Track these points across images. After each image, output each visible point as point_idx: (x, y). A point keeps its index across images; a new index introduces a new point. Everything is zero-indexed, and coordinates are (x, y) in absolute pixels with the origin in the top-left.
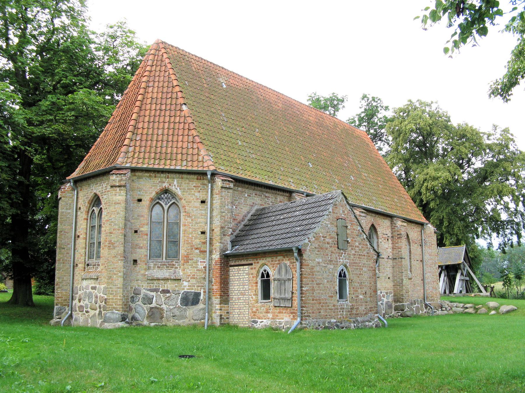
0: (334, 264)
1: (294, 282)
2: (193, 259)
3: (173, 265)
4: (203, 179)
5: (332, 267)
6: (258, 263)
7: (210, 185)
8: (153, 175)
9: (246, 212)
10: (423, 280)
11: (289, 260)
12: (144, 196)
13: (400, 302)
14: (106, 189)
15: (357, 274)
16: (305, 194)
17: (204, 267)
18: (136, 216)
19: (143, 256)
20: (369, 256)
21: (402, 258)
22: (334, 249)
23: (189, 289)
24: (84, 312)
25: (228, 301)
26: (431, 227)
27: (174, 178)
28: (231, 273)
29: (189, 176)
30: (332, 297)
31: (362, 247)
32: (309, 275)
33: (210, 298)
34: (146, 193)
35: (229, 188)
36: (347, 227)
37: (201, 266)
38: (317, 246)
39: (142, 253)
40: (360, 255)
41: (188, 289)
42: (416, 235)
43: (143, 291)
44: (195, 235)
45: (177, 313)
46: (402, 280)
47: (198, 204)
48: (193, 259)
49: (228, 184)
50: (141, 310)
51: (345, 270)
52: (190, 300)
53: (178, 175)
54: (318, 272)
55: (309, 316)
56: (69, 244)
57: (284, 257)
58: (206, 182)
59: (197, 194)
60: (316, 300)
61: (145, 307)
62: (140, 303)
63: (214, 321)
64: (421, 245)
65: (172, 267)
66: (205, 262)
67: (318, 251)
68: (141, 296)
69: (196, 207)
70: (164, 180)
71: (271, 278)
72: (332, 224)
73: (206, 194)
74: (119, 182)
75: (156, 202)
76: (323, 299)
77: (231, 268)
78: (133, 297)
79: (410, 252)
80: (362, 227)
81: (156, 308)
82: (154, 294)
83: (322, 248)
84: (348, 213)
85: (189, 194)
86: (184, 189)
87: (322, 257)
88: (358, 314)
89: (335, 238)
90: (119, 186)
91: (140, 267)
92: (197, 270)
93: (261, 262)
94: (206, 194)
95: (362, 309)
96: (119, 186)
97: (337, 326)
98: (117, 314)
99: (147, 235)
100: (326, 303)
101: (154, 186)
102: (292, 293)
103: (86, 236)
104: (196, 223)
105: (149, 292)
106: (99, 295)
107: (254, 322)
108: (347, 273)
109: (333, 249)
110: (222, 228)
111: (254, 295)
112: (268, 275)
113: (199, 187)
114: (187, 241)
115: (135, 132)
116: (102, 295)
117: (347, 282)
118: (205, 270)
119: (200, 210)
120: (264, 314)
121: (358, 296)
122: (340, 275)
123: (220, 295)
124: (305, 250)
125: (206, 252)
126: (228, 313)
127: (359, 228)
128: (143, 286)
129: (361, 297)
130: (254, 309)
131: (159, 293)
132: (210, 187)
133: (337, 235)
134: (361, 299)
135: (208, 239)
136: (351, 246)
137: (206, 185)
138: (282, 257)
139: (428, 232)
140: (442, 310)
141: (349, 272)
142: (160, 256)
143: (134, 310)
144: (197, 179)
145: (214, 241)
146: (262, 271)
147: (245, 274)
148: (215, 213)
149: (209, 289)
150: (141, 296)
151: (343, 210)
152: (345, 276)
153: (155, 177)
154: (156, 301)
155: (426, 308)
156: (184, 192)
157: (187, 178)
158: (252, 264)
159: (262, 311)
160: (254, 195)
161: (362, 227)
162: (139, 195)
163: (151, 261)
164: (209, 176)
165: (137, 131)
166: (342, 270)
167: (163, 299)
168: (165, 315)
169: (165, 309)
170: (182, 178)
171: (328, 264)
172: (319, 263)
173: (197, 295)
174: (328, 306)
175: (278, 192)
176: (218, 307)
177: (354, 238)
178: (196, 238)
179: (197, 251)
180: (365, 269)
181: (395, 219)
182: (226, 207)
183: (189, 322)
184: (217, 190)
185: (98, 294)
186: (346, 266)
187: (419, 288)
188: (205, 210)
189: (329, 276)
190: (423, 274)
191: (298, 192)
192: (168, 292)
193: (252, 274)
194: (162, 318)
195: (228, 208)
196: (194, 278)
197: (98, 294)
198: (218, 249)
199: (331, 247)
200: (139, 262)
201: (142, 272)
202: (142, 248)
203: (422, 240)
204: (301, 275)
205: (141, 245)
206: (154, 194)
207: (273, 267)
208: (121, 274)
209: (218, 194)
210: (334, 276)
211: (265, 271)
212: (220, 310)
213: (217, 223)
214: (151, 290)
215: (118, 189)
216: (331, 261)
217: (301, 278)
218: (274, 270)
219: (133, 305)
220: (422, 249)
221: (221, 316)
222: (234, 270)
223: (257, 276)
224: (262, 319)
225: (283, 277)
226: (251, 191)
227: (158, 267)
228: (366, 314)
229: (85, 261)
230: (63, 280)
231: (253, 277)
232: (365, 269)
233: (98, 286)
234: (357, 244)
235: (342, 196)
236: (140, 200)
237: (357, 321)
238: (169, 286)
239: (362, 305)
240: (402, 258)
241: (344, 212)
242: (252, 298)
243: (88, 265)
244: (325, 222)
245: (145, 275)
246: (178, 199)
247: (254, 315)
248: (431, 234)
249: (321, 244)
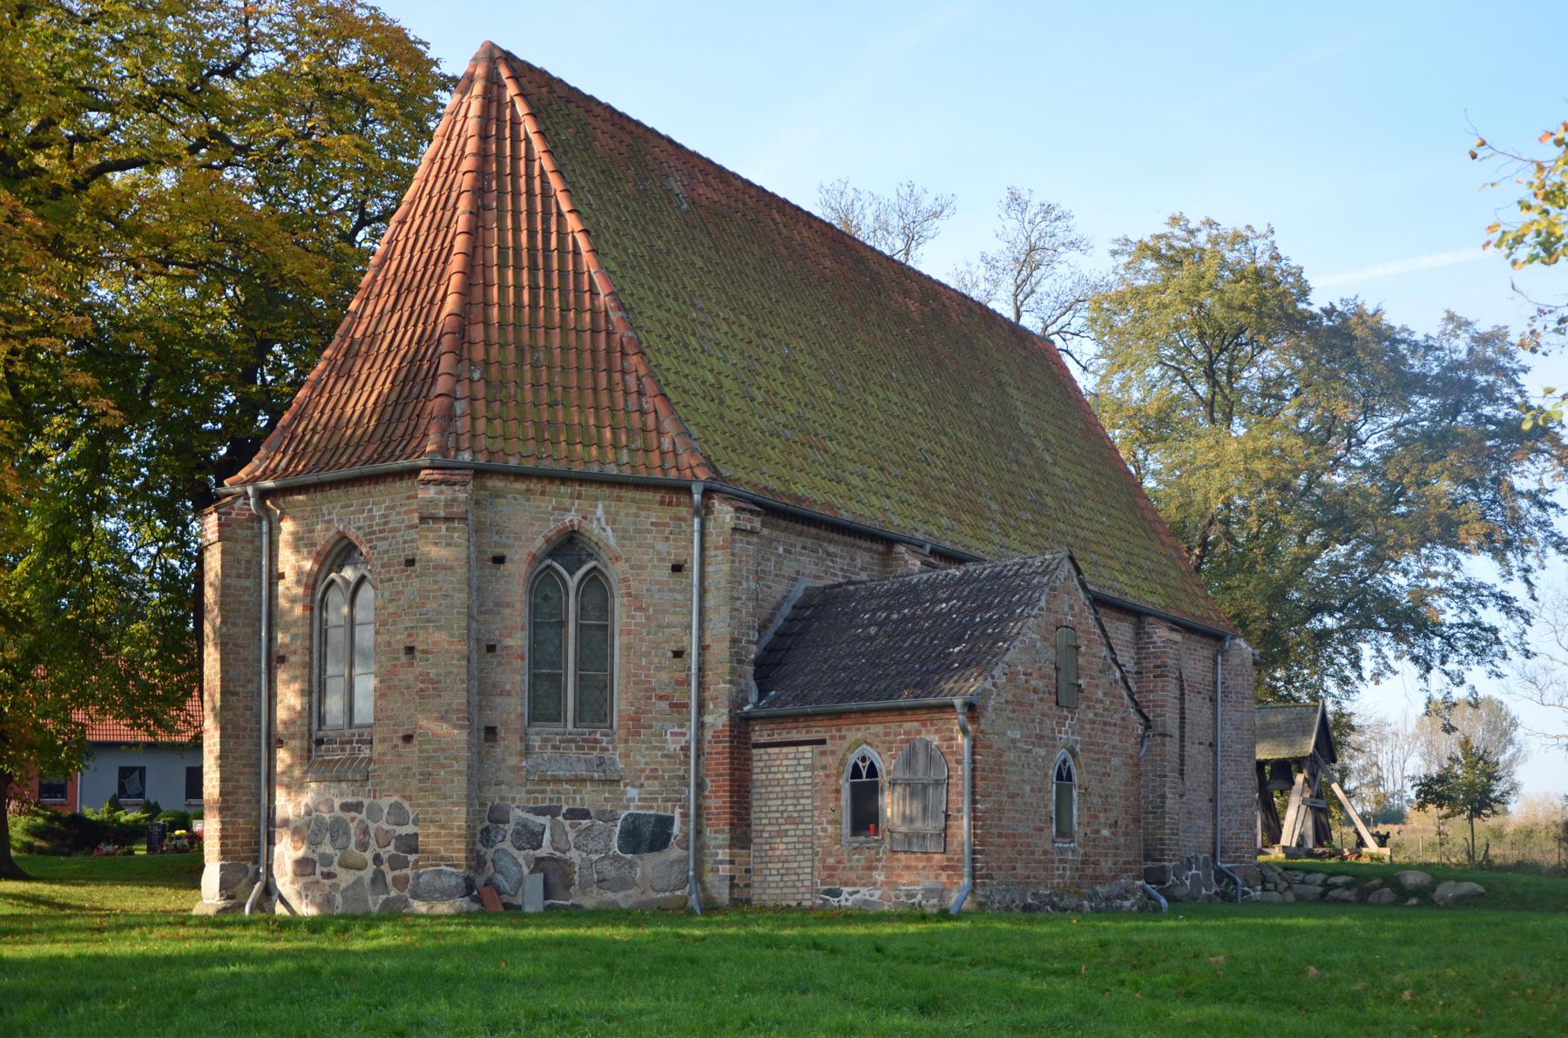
0: (1046, 745)
1: (953, 790)
2: (651, 727)
3: (596, 741)
4: (678, 504)
5: (1042, 752)
6: (843, 738)
7: (696, 520)
8: (535, 486)
9: (779, 597)
10: (1213, 800)
11: (936, 732)
12: (512, 547)
13: (1154, 860)
14: (386, 523)
15: (1096, 773)
16: (928, 548)
17: (682, 748)
18: (490, 605)
19: (513, 717)
20: (1126, 728)
21: (1164, 735)
22: (1049, 706)
23: (641, 808)
24: (318, 876)
25: (750, 841)
26: (1243, 645)
27: (597, 499)
28: (757, 766)
29: (637, 495)
30: (1041, 830)
31: (1112, 703)
32: (992, 771)
33: (699, 832)
34: (518, 538)
35: (752, 532)
36: (1077, 648)
37: (673, 745)
38: (1010, 697)
39: (512, 707)
40: (1105, 724)
41: (641, 808)
42: (1200, 666)
43: (517, 814)
44: (656, 660)
45: (610, 871)
46: (1163, 797)
47: (664, 573)
48: (651, 727)
49: (751, 521)
50: (515, 866)
51: (1071, 762)
52: (646, 835)
53: (607, 491)
54: (1013, 764)
55: (991, 877)
56: (249, 681)
57: (924, 725)
58: (684, 511)
59: (660, 546)
60: (1007, 836)
61: (520, 856)
62: (507, 845)
63: (714, 893)
64: (1213, 700)
65: (594, 749)
66: (684, 735)
67: (1014, 711)
68: (510, 828)
69: (658, 583)
70: (567, 502)
71: (883, 779)
72: (1046, 640)
73: (686, 547)
74: (446, 506)
75: (543, 565)
76: (1020, 836)
77: (755, 751)
78: (487, 830)
79: (1182, 718)
80: (1111, 649)
81: (551, 859)
82: (545, 820)
83: (1021, 704)
84: (1082, 611)
85: (640, 546)
86: (626, 531)
87: (1022, 727)
88: (1097, 878)
89: (1050, 677)
90: (447, 519)
91: (506, 747)
92: (664, 756)
93: (853, 734)
94: (686, 547)
95: (1106, 865)
96: (447, 519)
97: (1054, 907)
98: (453, 876)
99: (522, 658)
100: (1029, 845)
101: (540, 520)
102: (947, 817)
103: (311, 658)
104: (660, 626)
105: (531, 817)
106: (372, 827)
107: (830, 892)
108: (1074, 771)
109: (1044, 707)
110: (734, 641)
111: (829, 822)
112: (872, 771)
113: (666, 525)
114: (635, 675)
115: (465, 355)
116: (386, 827)
117: (1075, 793)
118: (687, 756)
119: (671, 590)
120: (860, 872)
121: (1098, 832)
122: (1059, 776)
123: (731, 824)
124: (985, 708)
125: (687, 706)
126: (747, 871)
127: (1105, 652)
128: (513, 799)
129: (1105, 833)
130: (831, 861)
131: (560, 818)
132: (696, 526)
133: (1057, 669)
134: (1105, 839)
135: (694, 671)
136: (1088, 699)
137: (685, 520)
138: (916, 724)
139: (1234, 661)
140: (1264, 890)
141: (1079, 767)
142: (558, 717)
143: (490, 864)
144: (662, 503)
145: (710, 677)
146: (853, 758)
147: (800, 768)
148: (711, 601)
149: (699, 807)
150: (510, 828)
151: (1074, 607)
152: (1069, 778)
153: (543, 493)
154: (553, 841)
155: (1219, 881)
156: (623, 538)
157: (633, 500)
158: (823, 742)
159: (854, 864)
160: (799, 549)
161: (1111, 649)
162: (497, 544)
163: (533, 730)
164: (697, 497)
165: (470, 351)
166: (1065, 762)
167: (571, 836)
168: (576, 877)
169: (578, 862)
170: (619, 499)
171: (1033, 744)
172: (1013, 741)
173: (665, 823)
174: (1033, 853)
175: (858, 542)
176: (723, 855)
177: (1092, 678)
178: (659, 669)
179: (664, 705)
180: (1115, 761)
181: (1151, 620)
182: (745, 585)
183: (644, 898)
184: (716, 536)
185: (369, 822)
186: (1072, 752)
187: (1201, 823)
188: (683, 591)
189: (1035, 775)
190: (1215, 781)
191: (908, 542)
192: (585, 814)
193: (824, 768)
194: (568, 885)
195: (748, 589)
196: (656, 778)
197: (369, 822)
198: (724, 700)
199: (1041, 700)
200: (501, 732)
201: (513, 761)
202: (509, 694)
203: (1215, 683)
204: (973, 770)
205: (508, 687)
206: (539, 543)
207: (890, 749)
208: (461, 766)
209: (722, 548)
210: (1046, 775)
211: (864, 759)
212: (731, 862)
213: (720, 626)
214: (539, 812)
215: (444, 527)
216: (1040, 737)
217: (973, 778)
218: (893, 757)
219: (489, 854)
220: (1215, 710)
221: (732, 878)
222: (765, 757)
223: (839, 775)
224: (854, 885)
225: (920, 775)
226: (792, 538)
227: (554, 747)
228: (1115, 877)
229: (310, 730)
230: (235, 787)
231: (827, 776)
232: (1115, 761)
233: (366, 802)
234: (1100, 694)
235: (1068, 565)
236: (499, 560)
237: (1096, 893)
238: (589, 797)
239: (1106, 855)
240: (1164, 735)
241: (1071, 608)
242: (824, 830)
243: (320, 742)
244: (1030, 634)
245: (521, 769)
246: (606, 558)
247: (831, 876)
248: (1243, 665)
249: (1019, 692)
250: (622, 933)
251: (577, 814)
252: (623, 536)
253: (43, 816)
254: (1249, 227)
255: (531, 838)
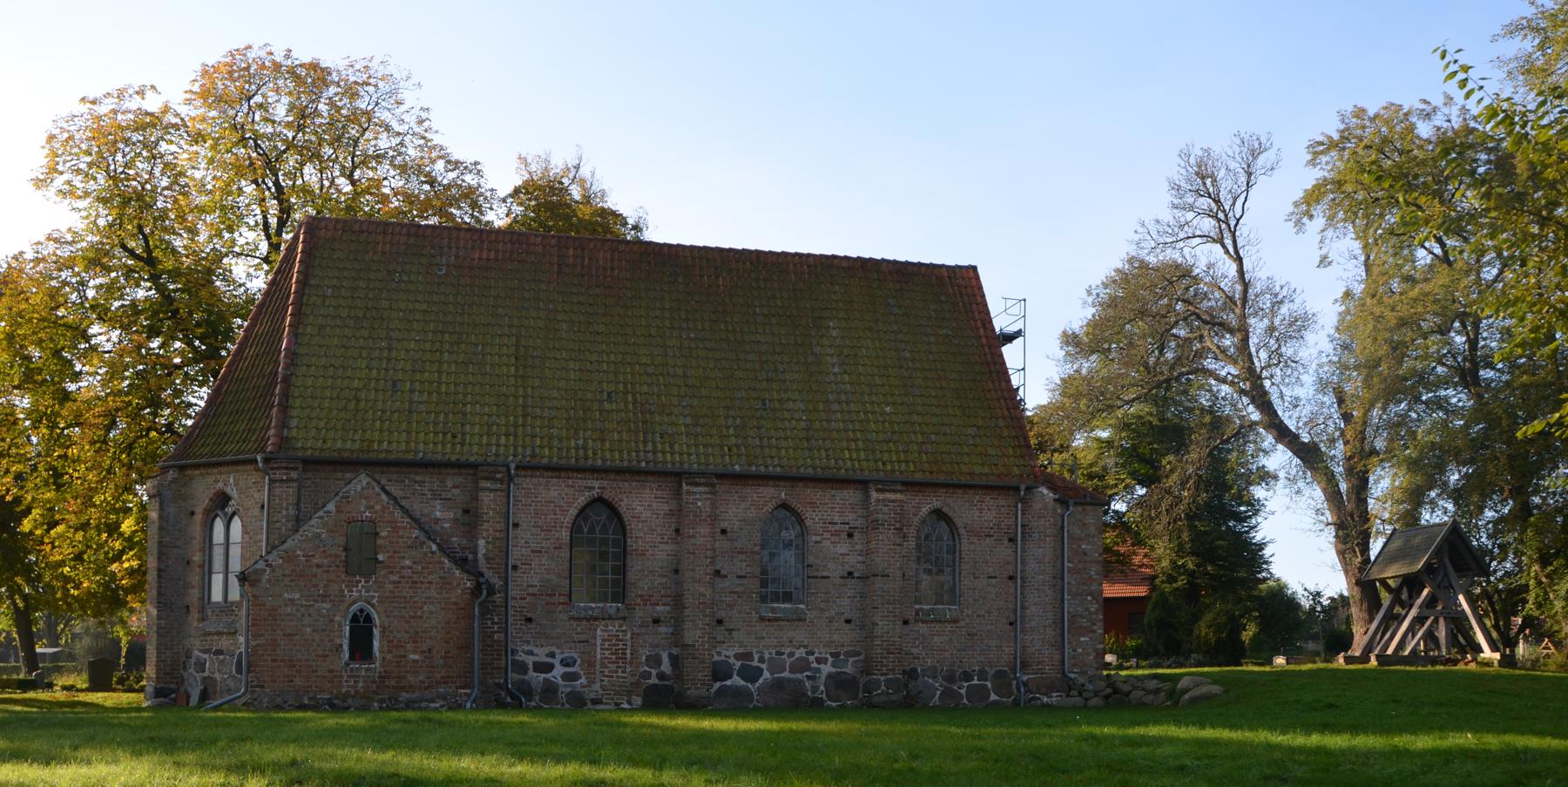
26: (1045, 491)
53: (231, 468)
62: (192, 670)
112: (368, 619)
139: (1037, 506)
214: (205, 652)
250: (18, 708)
251: (219, 652)
252: (241, 492)
253: (1186, 691)
254: (1425, 102)
255: (201, 666)
